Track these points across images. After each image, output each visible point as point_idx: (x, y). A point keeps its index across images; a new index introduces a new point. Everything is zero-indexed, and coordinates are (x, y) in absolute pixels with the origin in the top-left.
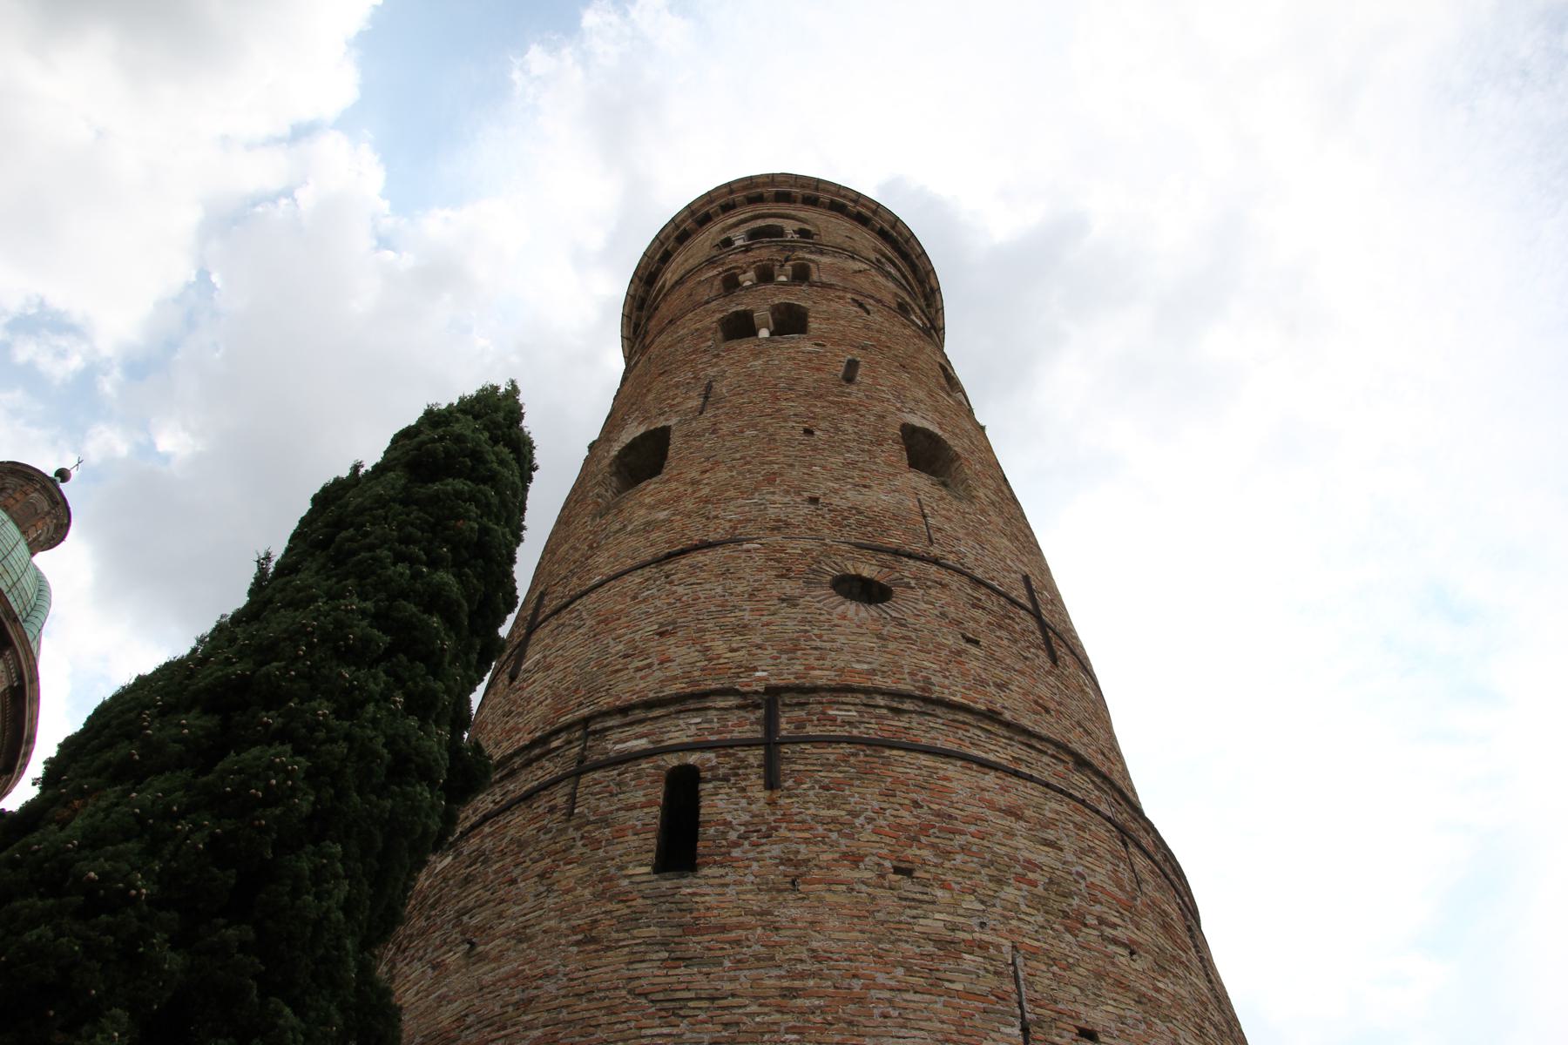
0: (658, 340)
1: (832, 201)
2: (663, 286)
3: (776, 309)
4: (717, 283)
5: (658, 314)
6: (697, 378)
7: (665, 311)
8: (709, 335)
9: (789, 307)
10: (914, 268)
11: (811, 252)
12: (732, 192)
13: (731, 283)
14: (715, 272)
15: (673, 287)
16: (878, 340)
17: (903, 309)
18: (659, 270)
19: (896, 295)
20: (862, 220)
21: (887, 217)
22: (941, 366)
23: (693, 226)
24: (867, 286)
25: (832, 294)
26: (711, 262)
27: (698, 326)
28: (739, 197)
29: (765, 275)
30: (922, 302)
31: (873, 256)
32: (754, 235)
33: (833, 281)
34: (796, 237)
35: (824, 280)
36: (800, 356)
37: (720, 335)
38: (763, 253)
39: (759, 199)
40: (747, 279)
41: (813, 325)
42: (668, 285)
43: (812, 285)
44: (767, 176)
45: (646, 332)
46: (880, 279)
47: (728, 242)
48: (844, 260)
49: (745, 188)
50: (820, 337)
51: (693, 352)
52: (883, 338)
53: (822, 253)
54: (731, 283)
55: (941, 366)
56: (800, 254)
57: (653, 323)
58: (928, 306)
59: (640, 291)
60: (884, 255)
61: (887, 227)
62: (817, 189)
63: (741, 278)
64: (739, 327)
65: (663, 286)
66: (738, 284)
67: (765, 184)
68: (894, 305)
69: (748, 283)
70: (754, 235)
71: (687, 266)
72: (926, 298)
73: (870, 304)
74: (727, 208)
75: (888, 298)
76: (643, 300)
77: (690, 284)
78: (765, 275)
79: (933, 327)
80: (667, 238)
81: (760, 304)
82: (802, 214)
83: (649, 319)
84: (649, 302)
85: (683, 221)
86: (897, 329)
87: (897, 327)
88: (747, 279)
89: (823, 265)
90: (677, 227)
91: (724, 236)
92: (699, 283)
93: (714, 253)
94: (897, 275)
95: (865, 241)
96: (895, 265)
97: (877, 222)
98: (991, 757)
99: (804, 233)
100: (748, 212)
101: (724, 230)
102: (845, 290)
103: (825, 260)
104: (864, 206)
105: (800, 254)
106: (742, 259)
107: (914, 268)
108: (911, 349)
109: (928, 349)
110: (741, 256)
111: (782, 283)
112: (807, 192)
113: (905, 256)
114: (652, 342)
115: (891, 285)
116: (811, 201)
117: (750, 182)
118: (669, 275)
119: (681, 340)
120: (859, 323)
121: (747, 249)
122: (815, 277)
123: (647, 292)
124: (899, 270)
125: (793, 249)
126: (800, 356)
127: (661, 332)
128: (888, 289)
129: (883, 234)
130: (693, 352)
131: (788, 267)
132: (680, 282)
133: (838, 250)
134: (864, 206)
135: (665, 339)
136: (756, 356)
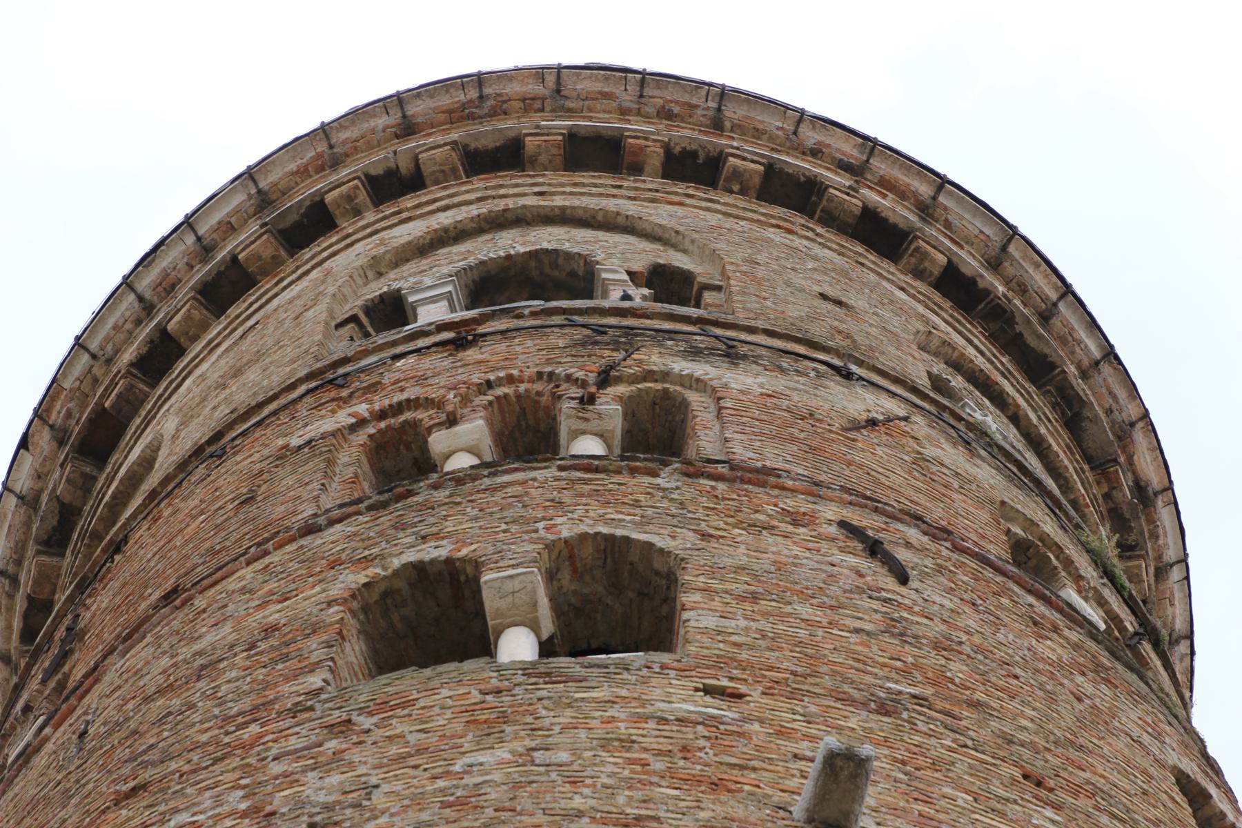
0: (117, 665)
1: (771, 170)
2: (147, 463)
3: (564, 559)
4: (350, 457)
5: (125, 569)
6: (94, 356)
7: (150, 555)
8: (314, 648)
9: (613, 552)
10: (1072, 412)
11: (694, 353)
12: (408, 129)
13: (401, 461)
14: (343, 418)
15: (184, 467)
16: (940, 680)
17: (1030, 562)
18: (130, 405)
19: (1004, 510)
20: (880, 237)
21: (976, 225)
22: (1184, 782)
23: (266, 247)
24: (898, 478)
25: (767, 504)
26: (328, 380)
27: (273, 614)
28: (434, 147)
29: (527, 435)
30: (1105, 538)
31: (919, 369)
32: (489, 287)
33: (773, 456)
34: (639, 295)
35: (741, 453)
36: (650, 736)
37: (354, 651)
38: (523, 352)
39: (508, 157)
40: (462, 444)
41: (699, 617)
42: (165, 462)
43: (693, 471)
44: (539, 73)
45: (75, 635)
46: (949, 453)
47: (391, 311)
48: (811, 371)
49: (457, 115)
50: (721, 663)
51: (253, 715)
52: (958, 670)
53: (731, 355)
54: (401, 461)
55: (1184, 782)
56: (654, 358)
57: (102, 599)
58: (1127, 550)
59: (58, 481)
60: (959, 365)
61: (971, 263)
62: (717, 125)
63: (438, 441)
64: (430, 621)
65: (147, 463)
66: (425, 465)
67: (529, 104)
68: (997, 550)
69: (462, 461)
70: (489, 287)
71: (241, 394)
72: (1118, 519)
73: (908, 543)
74: (389, 187)
75: (976, 525)
76: (67, 515)
77: (248, 459)
78: (527, 435)
79: (1149, 632)
80: (168, 287)
81: (509, 537)
82: (661, 215)
83: (84, 586)
84: (87, 521)
85: (227, 228)
86: (1012, 638)
87: (1007, 628)
88: (462, 444)
89: (734, 401)
90: (205, 249)
91: (378, 288)
92: (284, 454)
93: (341, 346)
94: (1009, 436)
95: (893, 314)
96: (999, 400)
97: (938, 247)
98: (213, 590)
99: (668, 284)
100: (469, 200)
101: (377, 267)
102: (815, 489)
103: (742, 381)
104: (886, 185)
105: (654, 358)
106: (440, 374)
107: (1072, 412)
108: (1067, 715)
109: (1132, 717)
110: (437, 362)
111: (589, 465)
112: (685, 135)
113: (1038, 369)
114: (94, 674)
115: (985, 474)
116: (695, 169)
117: (475, 94)
118: (167, 423)
119: (208, 668)
120: (869, 614)
121: (460, 338)
122: (705, 440)
123: (85, 484)
124: (1016, 419)
125: (629, 340)
126: (650, 736)
127: (131, 636)
128: (976, 489)
129: (956, 287)
130: (253, 715)
131: (610, 405)
132: (211, 450)
133: (797, 347)
134: (886, 185)
135: (148, 660)
136: (490, 728)
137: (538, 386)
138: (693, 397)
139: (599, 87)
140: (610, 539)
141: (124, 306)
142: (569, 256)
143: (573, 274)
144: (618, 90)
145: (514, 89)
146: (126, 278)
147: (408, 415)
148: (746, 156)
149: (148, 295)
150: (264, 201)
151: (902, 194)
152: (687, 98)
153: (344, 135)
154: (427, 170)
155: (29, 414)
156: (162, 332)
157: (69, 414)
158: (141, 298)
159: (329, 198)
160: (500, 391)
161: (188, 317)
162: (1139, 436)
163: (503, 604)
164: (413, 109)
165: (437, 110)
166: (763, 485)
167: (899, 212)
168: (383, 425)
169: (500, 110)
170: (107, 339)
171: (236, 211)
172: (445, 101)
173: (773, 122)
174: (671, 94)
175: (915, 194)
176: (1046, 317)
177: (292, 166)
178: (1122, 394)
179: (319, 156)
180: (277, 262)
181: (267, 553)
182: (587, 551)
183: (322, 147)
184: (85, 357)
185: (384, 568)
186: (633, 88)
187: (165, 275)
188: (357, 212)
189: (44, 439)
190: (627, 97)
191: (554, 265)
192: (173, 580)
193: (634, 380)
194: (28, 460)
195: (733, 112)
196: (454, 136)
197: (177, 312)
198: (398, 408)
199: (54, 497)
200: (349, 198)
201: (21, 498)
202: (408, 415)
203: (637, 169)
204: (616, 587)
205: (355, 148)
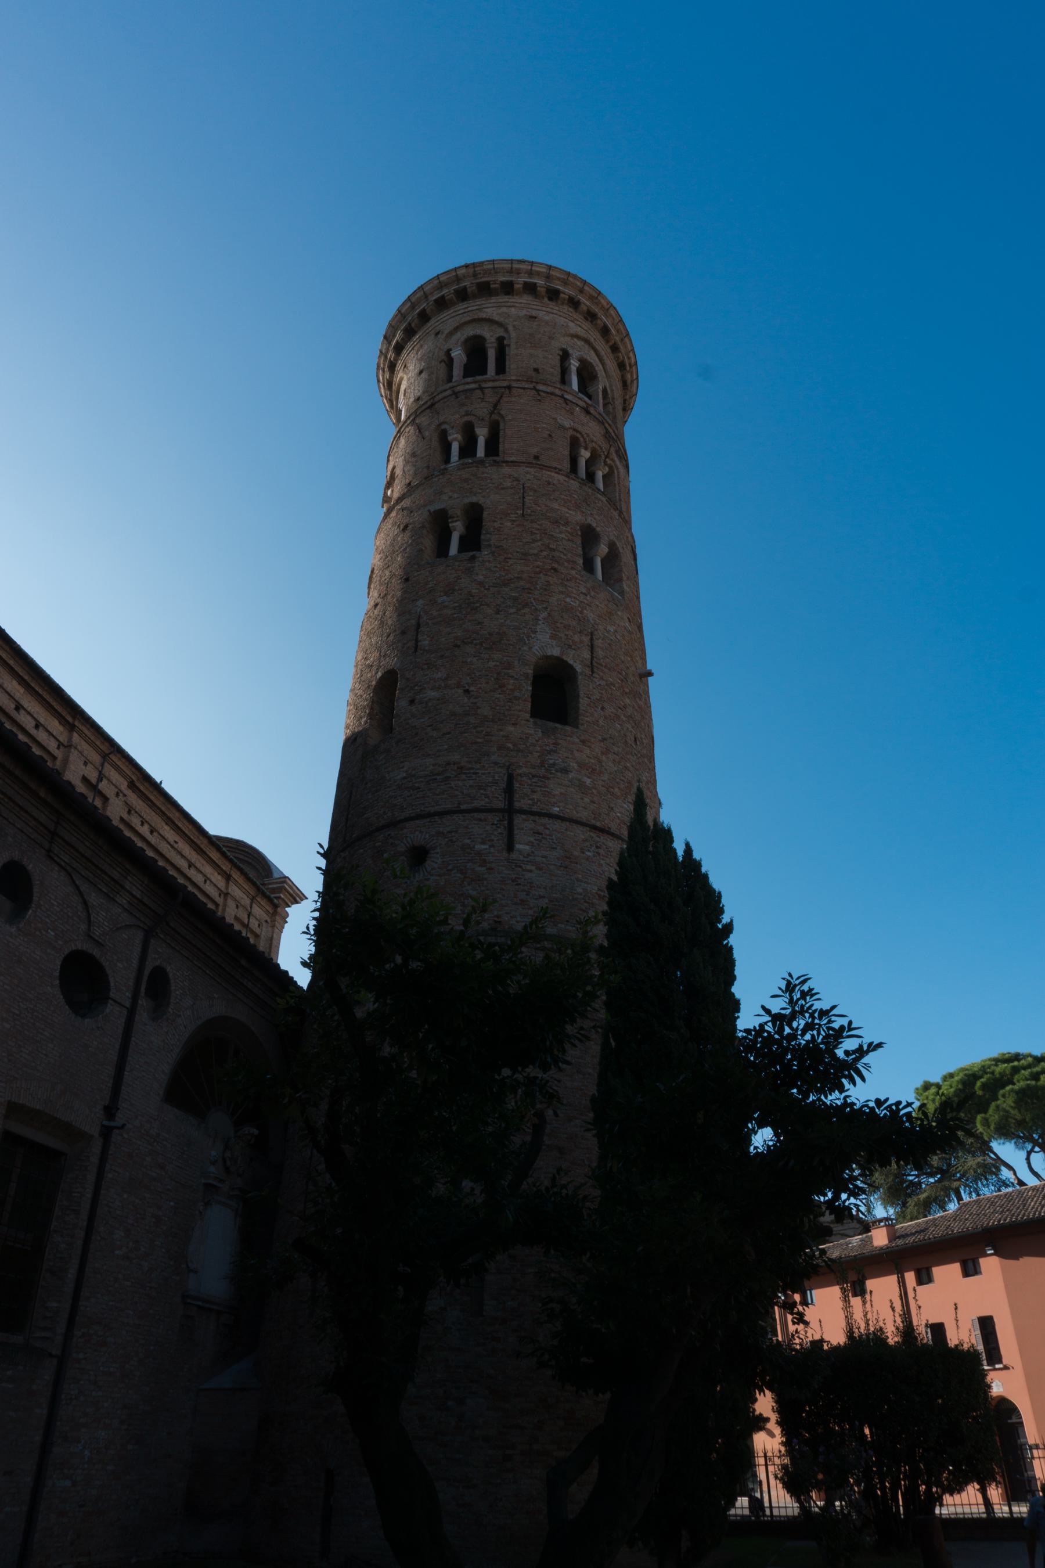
12: (581, 291)
85: (538, 273)
145: (602, 301)
147: (578, 435)
164: (586, 288)
194: (464, 271)
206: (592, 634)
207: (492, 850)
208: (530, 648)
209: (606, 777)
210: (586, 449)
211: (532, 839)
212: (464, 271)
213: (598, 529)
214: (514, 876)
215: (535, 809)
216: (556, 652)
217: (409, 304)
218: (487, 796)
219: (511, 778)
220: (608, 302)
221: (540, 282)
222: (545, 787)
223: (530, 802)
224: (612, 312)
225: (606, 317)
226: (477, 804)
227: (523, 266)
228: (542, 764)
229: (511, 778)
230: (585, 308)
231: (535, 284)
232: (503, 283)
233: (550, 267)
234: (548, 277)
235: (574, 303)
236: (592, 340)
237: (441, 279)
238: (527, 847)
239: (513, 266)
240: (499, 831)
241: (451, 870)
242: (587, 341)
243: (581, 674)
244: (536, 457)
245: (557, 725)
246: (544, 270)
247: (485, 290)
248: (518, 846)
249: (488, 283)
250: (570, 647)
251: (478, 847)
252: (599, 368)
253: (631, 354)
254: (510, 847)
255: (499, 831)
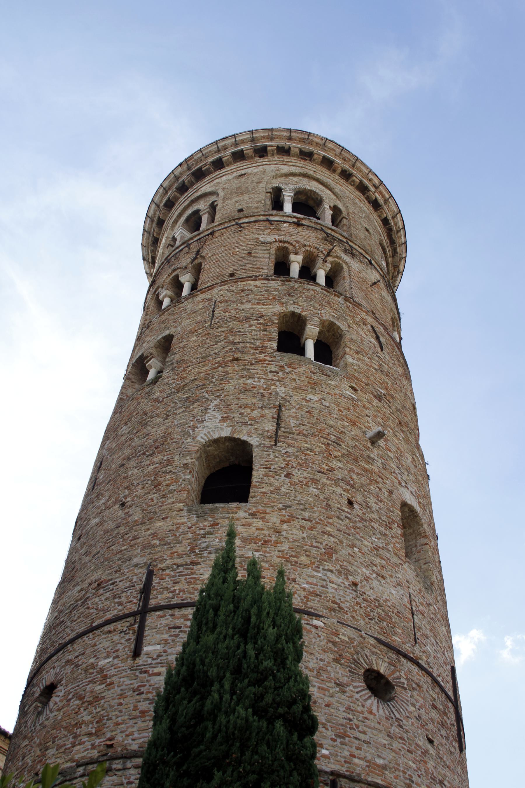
1: (361, 182)
12: (290, 139)
49: (302, 140)
62: (353, 166)
85: (243, 142)
90: (236, 144)
129: (385, 222)
134: (381, 193)
137: (314, 250)
138: (344, 266)
139: (333, 147)
140: (332, 322)
141: (214, 147)
142: (318, 194)
143: (317, 198)
144: (337, 149)
145: (315, 140)
146: (216, 141)
147: (286, 245)
148: (357, 176)
149: (220, 148)
150: (253, 140)
151: (383, 196)
152: (349, 157)
153: (276, 133)
154: (292, 152)
155: (184, 159)
156: (220, 159)
157: (193, 165)
158: (218, 148)
159: (269, 148)
160: (308, 248)
161: (228, 159)
162: (403, 261)
163: (310, 334)
164: (293, 134)
165: (298, 137)
166: (358, 308)
167: (381, 201)
168: (280, 244)
169: (311, 143)
170: (207, 153)
171: (246, 139)
172: (300, 136)
173: (364, 170)
174: (347, 155)
175: (385, 197)
176: (398, 231)
177: (262, 135)
178: (404, 251)
179: (269, 135)
180: (252, 157)
181: (256, 280)
182: (327, 323)
183: (270, 134)
184: (201, 154)
185: (287, 309)
186: (340, 150)
187: (225, 145)
188: (273, 155)
189: (185, 167)
190: (338, 151)
191: (314, 195)
192: (232, 269)
193: (334, 257)
194: (180, 169)
195: (358, 164)
196: (300, 146)
197: (226, 155)
198: (285, 242)
199: (183, 181)
200: (273, 151)
201: (175, 176)
202: (286, 245)
203: (334, 171)
204: (329, 331)
205: (278, 137)
206: (280, 407)
207: (116, 661)
208: (194, 438)
209: (285, 546)
210: (296, 253)
211: (166, 636)
212: (180, 169)
213: (303, 314)
214: (136, 685)
215: (174, 601)
216: (226, 433)
217: (149, 220)
218: (120, 604)
219: (150, 574)
220: (322, 138)
221: (246, 147)
222: (192, 573)
223: (171, 595)
224: (330, 145)
225: (325, 151)
226: (109, 616)
227: (226, 142)
228: (192, 550)
229: (150, 574)
230: (297, 150)
231: (242, 151)
232: (213, 163)
233: (252, 132)
234: (253, 140)
235: (284, 151)
236: (311, 173)
237: (164, 186)
238: (158, 647)
239: (218, 146)
240: (127, 637)
241: (70, 699)
242: (304, 175)
243: (257, 446)
244: (232, 275)
245: (217, 505)
246: (248, 136)
247: (199, 175)
248: (146, 649)
249: (200, 169)
250: (245, 424)
251: (103, 662)
252: (313, 186)
253: (371, 176)
254: (137, 653)
255: (127, 637)
